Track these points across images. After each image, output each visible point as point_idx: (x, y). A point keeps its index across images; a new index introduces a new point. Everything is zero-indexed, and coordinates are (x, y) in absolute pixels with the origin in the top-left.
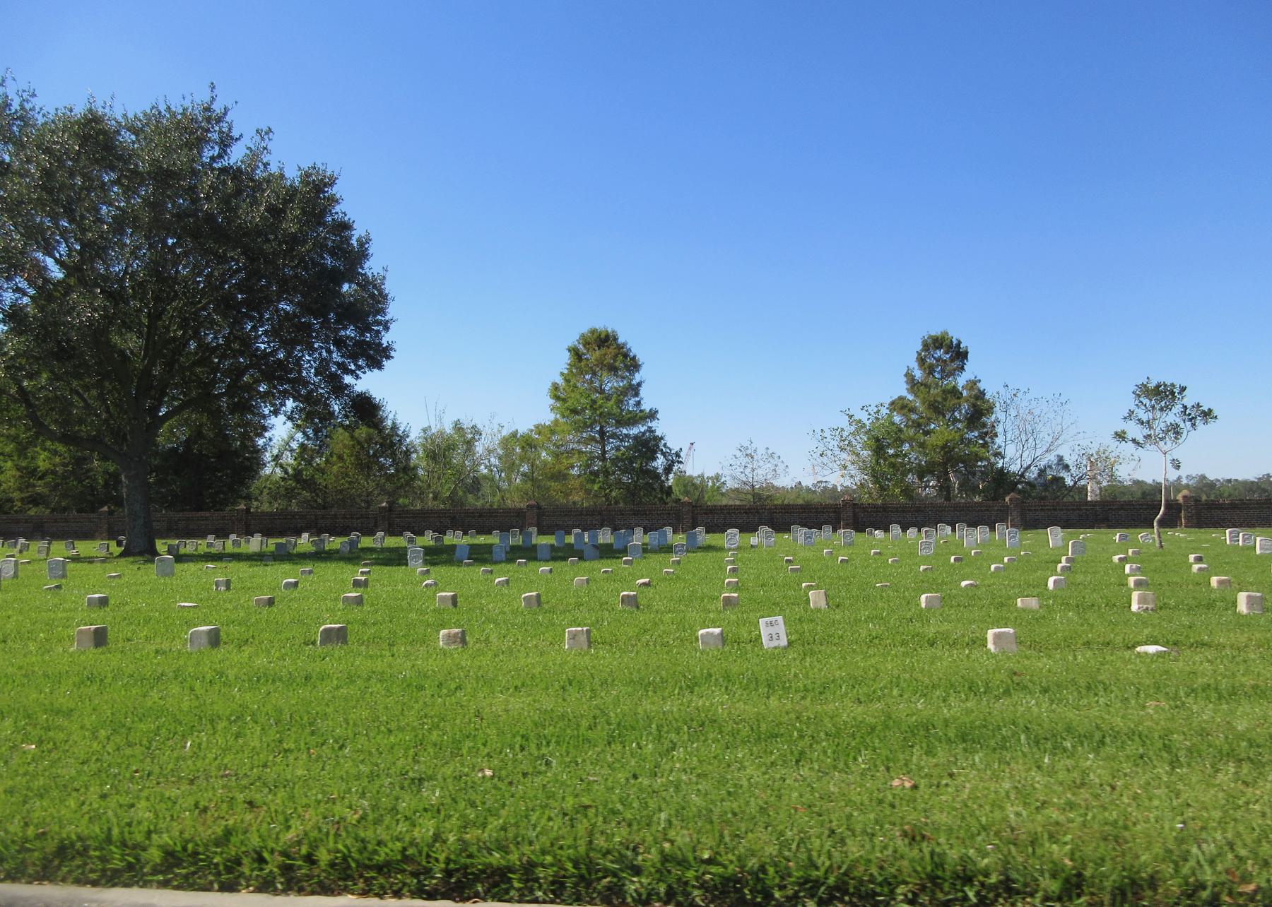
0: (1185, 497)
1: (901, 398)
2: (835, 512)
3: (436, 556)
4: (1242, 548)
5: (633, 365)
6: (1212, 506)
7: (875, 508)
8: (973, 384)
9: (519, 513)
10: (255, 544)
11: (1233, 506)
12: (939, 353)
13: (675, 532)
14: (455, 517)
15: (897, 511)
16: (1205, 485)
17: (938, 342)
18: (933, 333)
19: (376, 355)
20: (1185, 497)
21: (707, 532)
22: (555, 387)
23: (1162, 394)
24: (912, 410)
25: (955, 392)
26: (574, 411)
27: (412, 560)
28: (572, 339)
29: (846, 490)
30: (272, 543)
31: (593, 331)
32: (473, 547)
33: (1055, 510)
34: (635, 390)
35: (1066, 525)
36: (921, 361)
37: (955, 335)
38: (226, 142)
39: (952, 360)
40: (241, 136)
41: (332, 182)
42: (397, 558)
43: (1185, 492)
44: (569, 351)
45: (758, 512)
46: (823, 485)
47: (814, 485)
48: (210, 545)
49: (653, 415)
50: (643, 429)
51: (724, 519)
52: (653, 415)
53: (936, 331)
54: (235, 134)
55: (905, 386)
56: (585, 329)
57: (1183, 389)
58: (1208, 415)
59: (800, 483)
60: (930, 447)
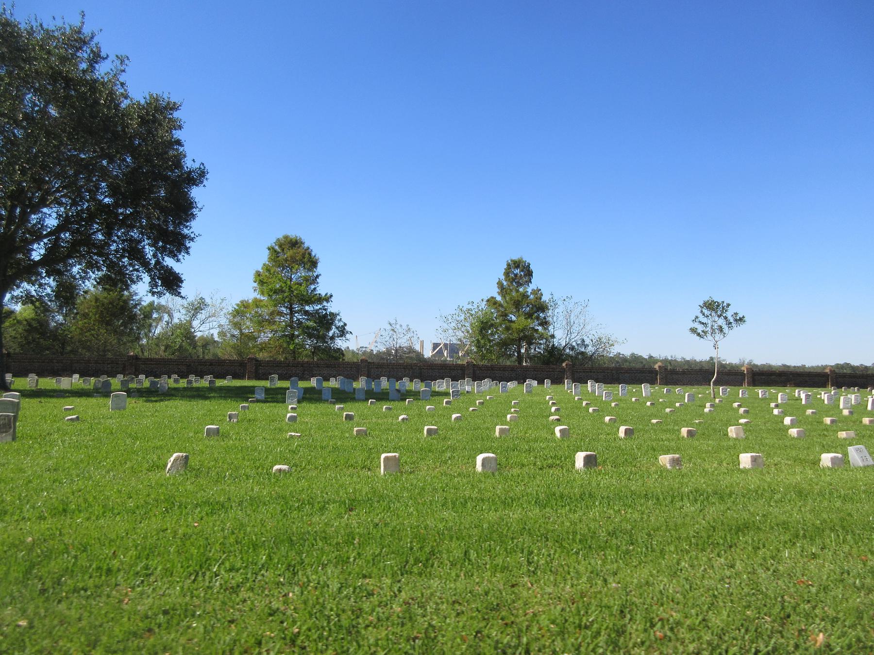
0: (659, 367)
1: (492, 298)
2: (462, 369)
3: (311, 396)
4: (762, 399)
5: (313, 263)
6: (673, 372)
7: (232, 362)
8: (537, 292)
9: (462, 367)
10: (75, 381)
11: (684, 373)
12: (517, 271)
13: (411, 381)
14: (190, 365)
15: (500, 370)
16: (635, 358)
17: (517, 264)
18: (514, 258)
19: (304, 243)
20: (659, 367)
21: (279, 379)
22: (258, 274)
23: (711, 306)
24: (501, 305)
25: (525, 296)
26: (276, 292)
27: (289, 398)
28: (271, 241)
29: (379, 353)
30: (92, 382)
31: (286, 237)
32: (267, 391)
33: (591, 372)
34: (314, 280)
35: (597, 381)
36: (507, 274)
37: (527, 259)
38: (96, 57)
39: (525, 275)
40: (108, 56)
41: (174, 107)
42: (276, 396)
43: (659, 364)
44: (269, 249)
45: (412, 368)
46: (364, 349)
47: (358, 349)
48: (190, 382)
49: (328, 298)
50: (319, 306)
51: (390, 372)
52: (328, 298)
53: (516, 257)
54: (103, 54)
55: (498, 290)
56: (280, 236)
57: (728, 305)
58: (741, 320)
59: (348, 348)
60: (514, 330)
